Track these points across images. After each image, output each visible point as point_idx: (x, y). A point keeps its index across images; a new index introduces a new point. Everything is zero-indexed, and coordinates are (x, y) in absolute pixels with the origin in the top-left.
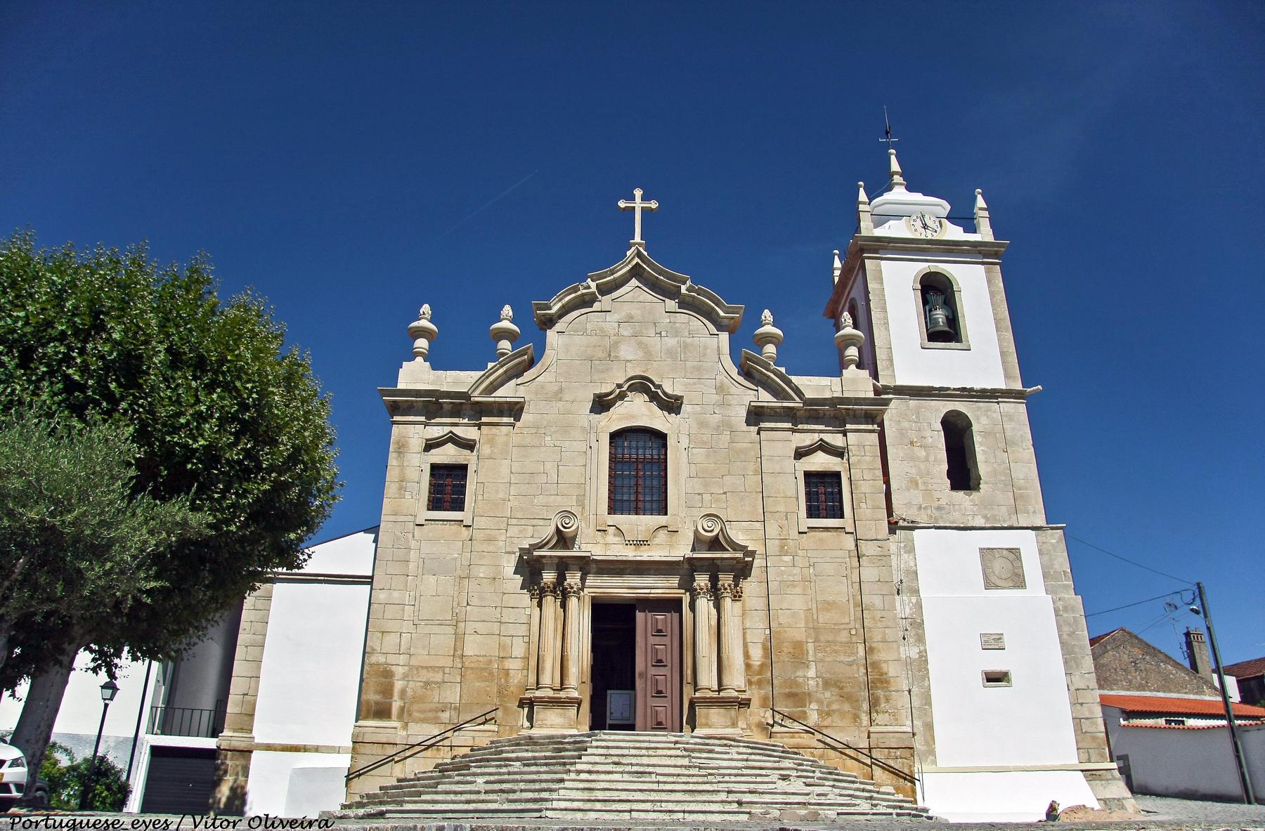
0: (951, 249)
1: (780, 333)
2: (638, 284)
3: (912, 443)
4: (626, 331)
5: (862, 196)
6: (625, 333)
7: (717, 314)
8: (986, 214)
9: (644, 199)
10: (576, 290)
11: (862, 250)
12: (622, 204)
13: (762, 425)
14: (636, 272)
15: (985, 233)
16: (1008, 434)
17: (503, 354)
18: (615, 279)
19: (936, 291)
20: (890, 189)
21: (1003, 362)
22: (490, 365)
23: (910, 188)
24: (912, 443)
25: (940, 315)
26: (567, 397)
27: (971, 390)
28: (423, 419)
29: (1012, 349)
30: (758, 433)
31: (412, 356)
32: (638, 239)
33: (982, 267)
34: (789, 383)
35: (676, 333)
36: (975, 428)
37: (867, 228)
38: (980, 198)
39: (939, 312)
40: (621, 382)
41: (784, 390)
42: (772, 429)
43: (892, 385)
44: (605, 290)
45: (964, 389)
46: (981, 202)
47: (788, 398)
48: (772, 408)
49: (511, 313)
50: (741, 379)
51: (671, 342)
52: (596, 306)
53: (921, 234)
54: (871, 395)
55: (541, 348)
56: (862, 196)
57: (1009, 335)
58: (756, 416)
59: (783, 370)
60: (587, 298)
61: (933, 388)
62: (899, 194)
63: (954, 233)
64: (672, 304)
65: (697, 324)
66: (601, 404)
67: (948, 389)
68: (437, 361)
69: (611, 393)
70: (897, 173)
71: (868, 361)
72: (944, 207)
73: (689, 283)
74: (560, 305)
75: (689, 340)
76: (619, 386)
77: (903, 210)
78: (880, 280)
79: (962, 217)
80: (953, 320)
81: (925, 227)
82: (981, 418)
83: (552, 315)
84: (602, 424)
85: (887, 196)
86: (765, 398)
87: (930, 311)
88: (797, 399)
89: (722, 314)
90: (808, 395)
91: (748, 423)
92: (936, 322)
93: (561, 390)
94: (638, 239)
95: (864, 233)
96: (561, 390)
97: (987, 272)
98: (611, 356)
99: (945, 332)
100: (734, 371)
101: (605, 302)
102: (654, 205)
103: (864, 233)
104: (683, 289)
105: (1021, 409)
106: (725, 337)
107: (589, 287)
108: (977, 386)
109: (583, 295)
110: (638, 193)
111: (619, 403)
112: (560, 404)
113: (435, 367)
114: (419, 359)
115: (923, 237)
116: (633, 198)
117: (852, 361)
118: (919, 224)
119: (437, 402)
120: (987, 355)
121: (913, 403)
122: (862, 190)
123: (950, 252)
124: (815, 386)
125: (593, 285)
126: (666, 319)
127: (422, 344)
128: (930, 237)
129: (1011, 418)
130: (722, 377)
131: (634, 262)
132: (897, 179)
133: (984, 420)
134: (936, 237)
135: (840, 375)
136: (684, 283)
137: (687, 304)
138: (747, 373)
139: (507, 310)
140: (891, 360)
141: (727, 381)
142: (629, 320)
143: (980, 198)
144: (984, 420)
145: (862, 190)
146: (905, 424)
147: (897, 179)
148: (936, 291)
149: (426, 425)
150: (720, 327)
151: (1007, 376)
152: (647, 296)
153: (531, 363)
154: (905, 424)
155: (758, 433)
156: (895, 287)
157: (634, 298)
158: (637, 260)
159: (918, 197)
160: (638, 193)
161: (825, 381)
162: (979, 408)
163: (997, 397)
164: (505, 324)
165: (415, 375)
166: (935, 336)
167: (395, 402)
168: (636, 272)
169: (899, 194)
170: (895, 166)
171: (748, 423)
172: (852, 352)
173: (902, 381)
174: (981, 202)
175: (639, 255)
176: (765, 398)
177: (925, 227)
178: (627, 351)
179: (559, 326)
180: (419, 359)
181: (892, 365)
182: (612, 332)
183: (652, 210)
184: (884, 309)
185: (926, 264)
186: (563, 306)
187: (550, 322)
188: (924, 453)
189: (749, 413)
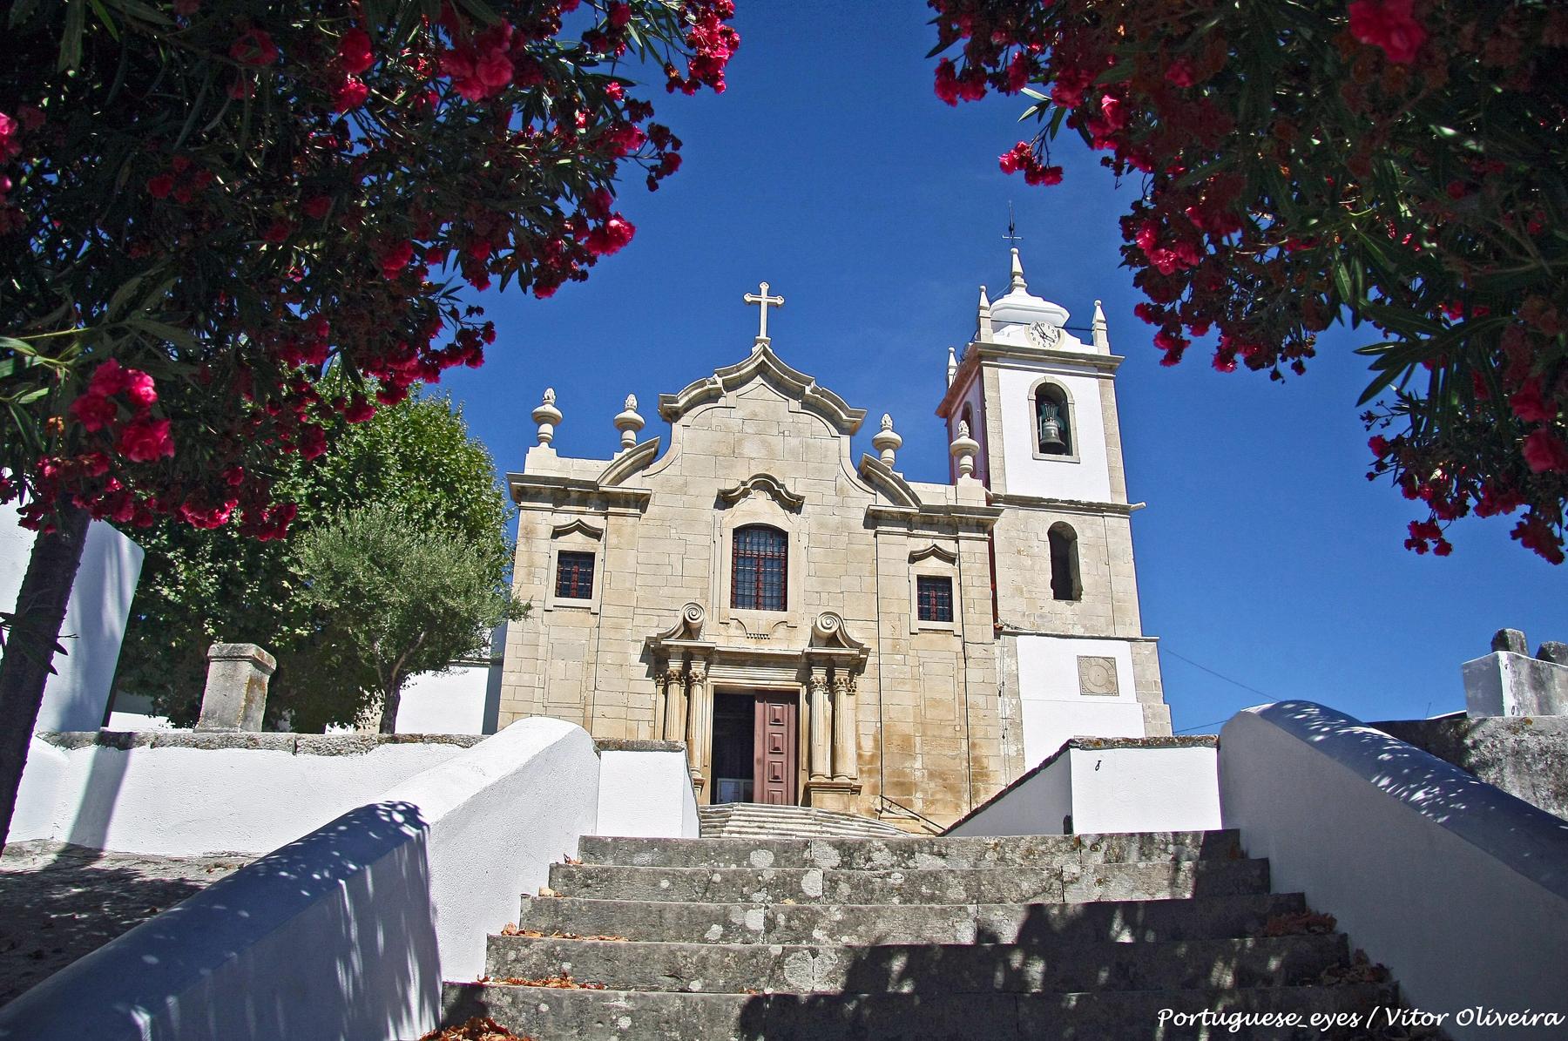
8: (1104, 326)
10: (702, 384)
12: (748, 298)
13: (523, 504)
14: (761, 370)
15: (1101, 348)
19: (1050, 401)
25: (1053, 426)
27: (1078, 503)
28: (550, 505)
31: (540, 441)
32: (763, 335)
34: (907, 489)
35: (799, 434)
42: (889, 533)
44: (731, 386)
47: (904, 503)
50: (860, 483)
51: (794, 442)
52: (722, 402)
53: (1038, 344)
62: (1019, 297)
63: (1071, 344)
64: (795, 404)
65: (819, 425)
68: (564, 449)
71: (982, 472)
72: (1063, 315)
76: (744, 483)
77: (1022, 316)
79: (1080, 328)
80: (1065, 432)
81: (1044, 336)
82: (1085, 530)
86: (883, 503)
94: (763, 335)
99: (1057, 445)
100: (854, 474)
101: (729, 398)
102: (779, 301)
103: (984, 340)
104: (808, 390)
108: (1085, 499)
110: (764, 287)
112: (685, 498)
114: (544, 445)
115: (1041, 347)
117: (544, 439)
119: (565, 490)
121: (1022, 513)
123: (1066, 364)
124: (932, 494)
125: (720, 381)
126: (789, 418)
127: (547, 429)
130: (842, 480)
132: (1018, 280)
133: (1089, 533)
134: (1055, 348)
137: (808, 405)
138: (866, 477)
142: (753, 417)
148: (1050, 401)
149: (554, 512)
152: (770, 394)
156: (1010, 395)
158: (763, 358)
159: (1038, 302)
160: (764, 287)
161: (940, 488)
166: (1046, 448)
168: (761, 370)
169: (1019, 297)
172: (967, 461)
176: (883, 503)
177: (1044, 336)
178: (750, 449)
179: (685, 419)
180: (544, 445)
187: (675, 415)
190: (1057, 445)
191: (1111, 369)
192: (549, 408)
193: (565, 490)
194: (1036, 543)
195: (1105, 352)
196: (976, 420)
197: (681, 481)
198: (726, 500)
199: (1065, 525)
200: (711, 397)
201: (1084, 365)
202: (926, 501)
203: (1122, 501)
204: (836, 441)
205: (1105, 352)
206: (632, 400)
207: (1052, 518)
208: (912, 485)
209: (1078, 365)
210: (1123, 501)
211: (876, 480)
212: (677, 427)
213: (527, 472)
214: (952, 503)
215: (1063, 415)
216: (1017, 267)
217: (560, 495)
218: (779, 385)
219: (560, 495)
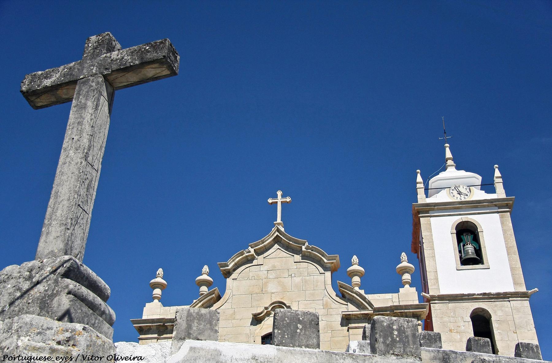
0: (477, 205)
1: (109, 291)
2: (279, 247)
3: (451, 331)
4: (272, 275)
5: (419, 179)
6: (271, 277)
7: (323, 261)
8: (501, 180)
9: (283, 196)
10: (242, 254)
11: (419, 212)
12: (270, 201)
13: (350, 325)
14: (277, 240)
15: (500, 193)
16: (517, 321)
17: (202, 294)
18: (265, 246)
19: (466, 233)
20: (445, 169)
21: (513, 275)
22: (195, 301)
23: (458, 168)
24: (451, 331)
25: (470, 248)
26: (237, 317)
27: (489, 294)
28: (156, 336)
29: (519, 265)
30: (348, 331)
31: (151, 299)
32: (279, 220)
33: (497, 215)
34: (364, 299)
35: (301, 275)
36: (493, 319)
37: (422, 199)
38: (497, 170)
39: (469, 246)
40: (267, 306)
41: (362, 303)
42: (356, 328)
43: (436, 294)
44: (259, 253)
45: (484, 294)
46: (497, 173)
47: (365, 308)
48: (355, 315)
49: (208, 270)
50: (338, 299)
51: (297, 280)
52: (255, 262)
53: (457, 198)
54: (417, 302)
55: (223, 289)
56: (419, 179)
57: (517, 257)
58: (347, 320)
59: (362, 292)
60: (249, 258)
61: (464, 295)
62: (451, 172)
63: (480, 195)
64: (298, 258)
65: (312, 268)
66: (257, 320)
67: (474, 294)
68: (166, 302)
69: (261, 313)
70: (449, 159)
71: (421, 281)
72: (477, 179)
73: (307, 244)
74: (233, 263)
75: (308, 278)
76: (266, 308)
77: (454, 182)
78: (430, 230)
79: (487, 186)
80: (478, 251)
81: (460, 193)
82: (497, 312)
83: (229, 270)
84: (257, 331)
85: (442, 175)
86: (352, 309)
87: (464, 246)
88: (370, 308)
89: (326, 261)
90: (376, 306)
91: (342, 325)
92: (467, 253)
93: (234, 313)
94: (279, 220)
95: (420, 202)
96: (234, 313)
97: (501, 217)
98: (262, 291)
99: (474, 259)
100: (333, 294)
101: (260, 259)
102: (288, 199)
103: (420, 202)
104: (304, 248)
105: (526, 304)
106: (328, 274)
107: (250, 252)
108: (494, 291)
109: (247, 256)
110: (279, 193)
111: (267, 318)
112: (234, 321)
113: (165, 305)
114: (156, 301)
115: (459, 200)
116: (276, 197)
117: (407, 283)
118: (455, 192)
119: (164, 325)
120: (501, 268)
121: (451, 305)
122: (419, 175)
123: (476, 207)
124: (380, 300)
125: (252, 250)
126: (295, 266)
127: (157, 292)
128: (463, 200)
129: (518, 310)
130: (327, 299)
131: (275, 235)
132: (450, 162)
133: (500, 313)
134: (468, 199)
135: (398, 291)
136: (304, 245)
137: (306, 257)
138: (343, 296)
139: (206, 269)
140: (437, 279)
141: (330, 300)
142: (273, 269)
143: (497, 170)
144: (500, 313)
145: (419, 175)
146: (446, 319)
147: (450, 162)
148: (466, 233)
149: (158, 339)
150: (326, 269)
151: (515, 283)
152: (283, 254)
153: (219, 298)
154: (446, 319)
155: (348, 331)
156: (439, 234)
157: (277, 253)
158: (277, 233)
159: (462, 173)
160: (279, 193)
161: (388, 296)
162: (496, 306)
163: (509, 298)
164: (205, 277)
165: (153, 311)
166: (466, 261)
167: (140, 327)
168: (277, 240)
169: (451, 172)
170: (448, 154)
171: (342, 325)
172: (407, 277)
173: (444, 291)
174: (497, 173)
175: (278, 230)
176: (352, 309)
177: (460, 193)
178: (272, 287)
179: (234, 276)
180: (156, 301)
181: (437, 282)
182: (264, 277)
183: (288, 202)
184: (433, 249)
185: (460, 217)
186: (236, 264)
187: (228, 274)
188: (459, 337)
189: (343, 319)
190: (474, 259)
191: (507, 206)
192: (356, 267)
193: (164, 325)
194: (462, 324)
195: (503, 196)
196: (417, 249)
197: (231, 312)
198: (257, 320)
199: (483, 310)
200: (249, 260)
201: (488, 206)
202: (376, 305)
203: (523, 289)
204: (323, 276)
205: (503, 196)
206: (355, 259)
207: (473, 306)
208: (369, 297)
209: (484, 207)
210: (523, 289)
211: (347, 296)
212: (229, 281)
213: (144, 317)
214: (395, 304)
215: (476, 239)
216: (448, 154)
217: (162, 329)
218: (288, 248)
219: (162, 329)
